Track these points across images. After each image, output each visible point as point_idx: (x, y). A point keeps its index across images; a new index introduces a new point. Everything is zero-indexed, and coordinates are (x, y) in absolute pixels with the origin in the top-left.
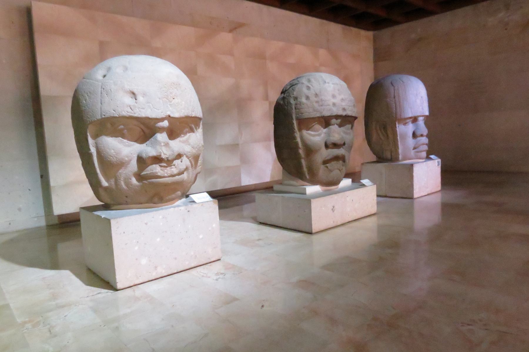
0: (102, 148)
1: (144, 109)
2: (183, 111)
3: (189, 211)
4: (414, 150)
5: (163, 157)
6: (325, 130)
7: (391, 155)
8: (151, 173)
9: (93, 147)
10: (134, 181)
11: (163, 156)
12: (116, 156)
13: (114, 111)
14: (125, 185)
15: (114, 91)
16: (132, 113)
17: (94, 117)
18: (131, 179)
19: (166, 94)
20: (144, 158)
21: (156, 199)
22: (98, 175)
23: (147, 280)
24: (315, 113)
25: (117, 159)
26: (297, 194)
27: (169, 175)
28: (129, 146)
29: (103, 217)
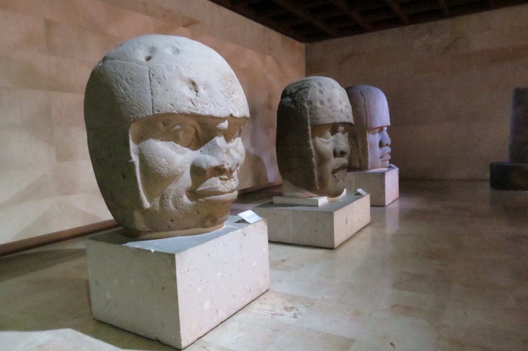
0: (150, 155)
1: (207, 104)
2: (242, 109)
3: (244, 234)
4: (381, 159)
5: (226, 168)
6: (332, 138)
7: (360, 165)
8: (211, 188)
9: (135, 154)
10: (186, 199)
11: (226, 167)
12: (168, 166)
13: (172, 105)
14: (174, 205)
15: (168, 78)
16: (195, 110)
17: (143, 113)
18: (182, 197)
19: (226, 86)
20: (205, 168)
21: (208, 222)
22: (140, 193)
23: (209, 330)
24: (330, 119)
25: (170, 171)
26: (311, 207)
27: (229, 190)
28: (182, 153)
29: (153, 251)
